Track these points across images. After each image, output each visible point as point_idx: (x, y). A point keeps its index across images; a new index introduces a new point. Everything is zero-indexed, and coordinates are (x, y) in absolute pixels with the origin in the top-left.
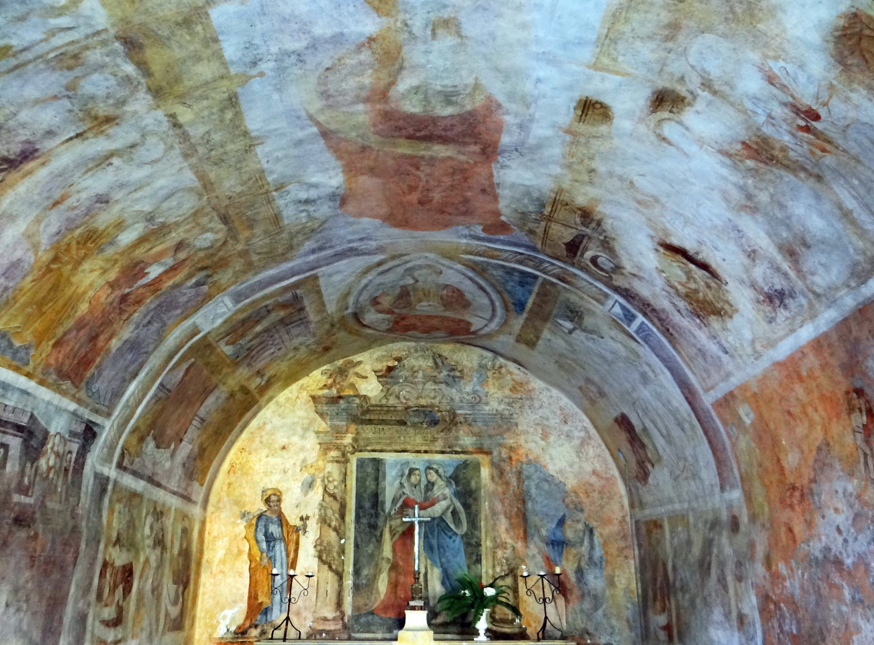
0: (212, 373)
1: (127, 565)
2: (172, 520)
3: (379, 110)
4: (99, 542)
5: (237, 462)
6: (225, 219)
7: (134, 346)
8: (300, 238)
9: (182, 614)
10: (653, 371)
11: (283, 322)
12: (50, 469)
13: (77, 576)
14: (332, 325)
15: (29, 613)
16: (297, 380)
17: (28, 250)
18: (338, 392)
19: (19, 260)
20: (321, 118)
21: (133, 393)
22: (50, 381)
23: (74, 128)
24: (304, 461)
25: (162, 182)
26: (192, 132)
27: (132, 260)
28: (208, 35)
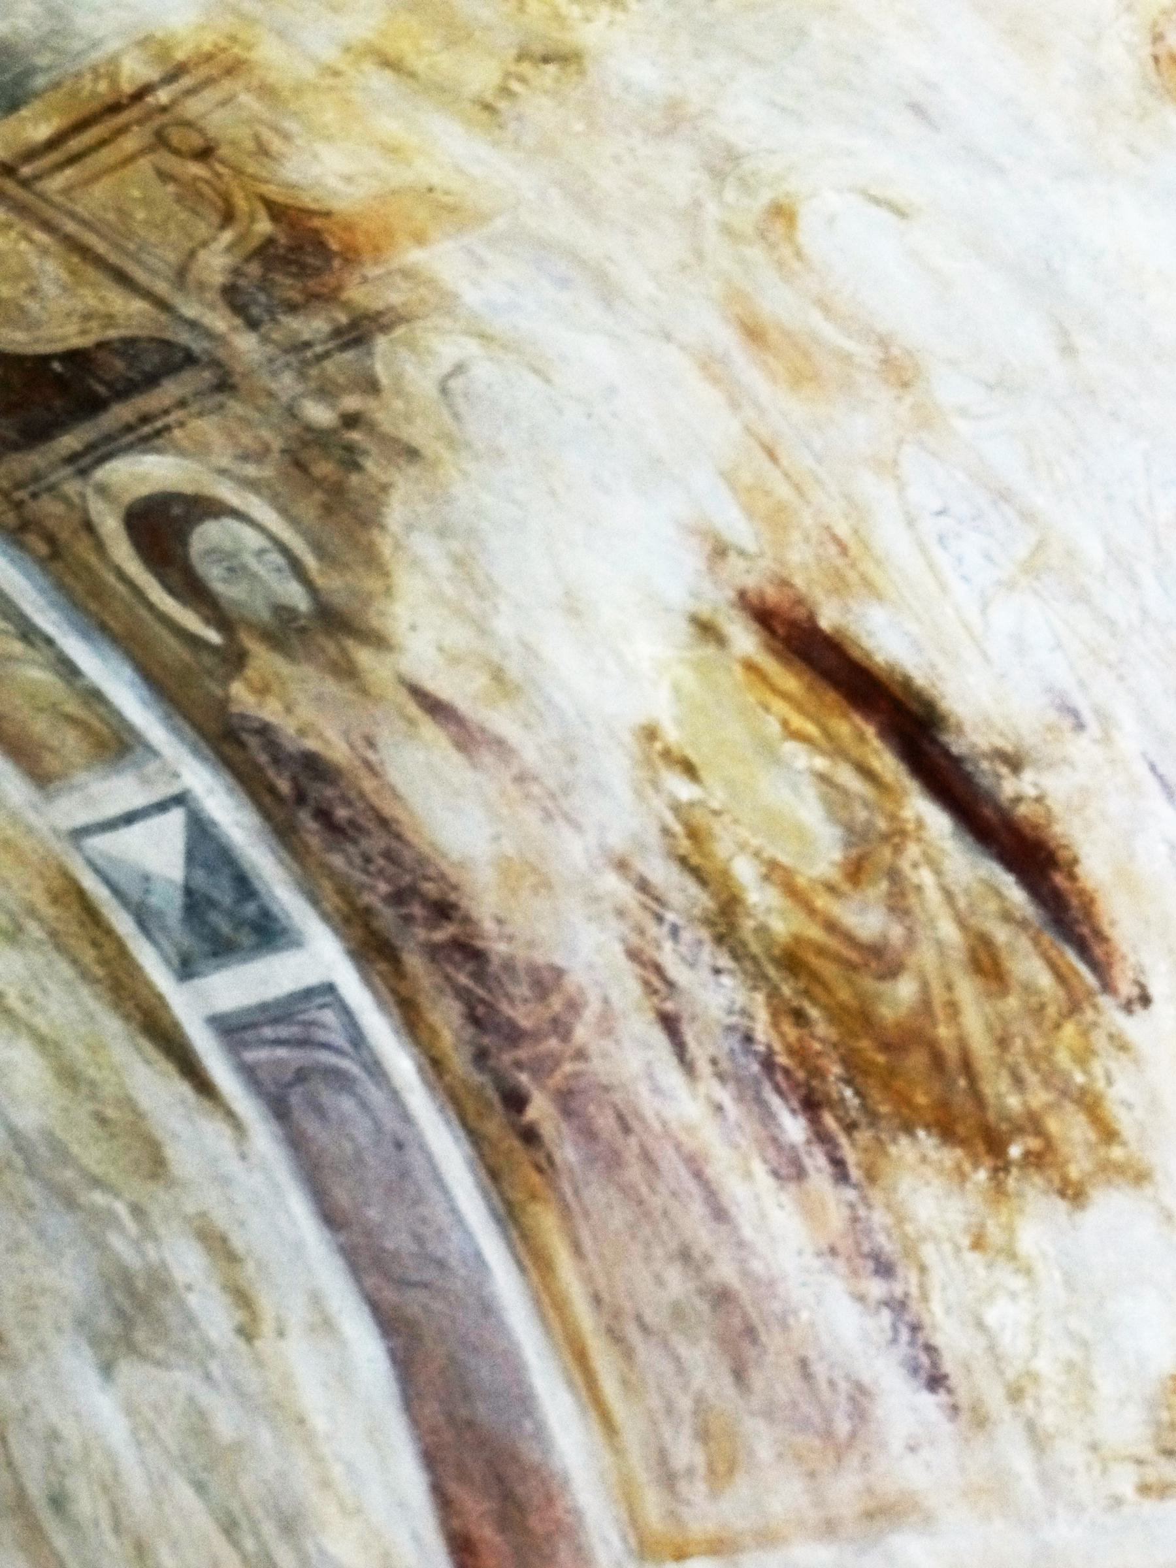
10: (242, 1298)
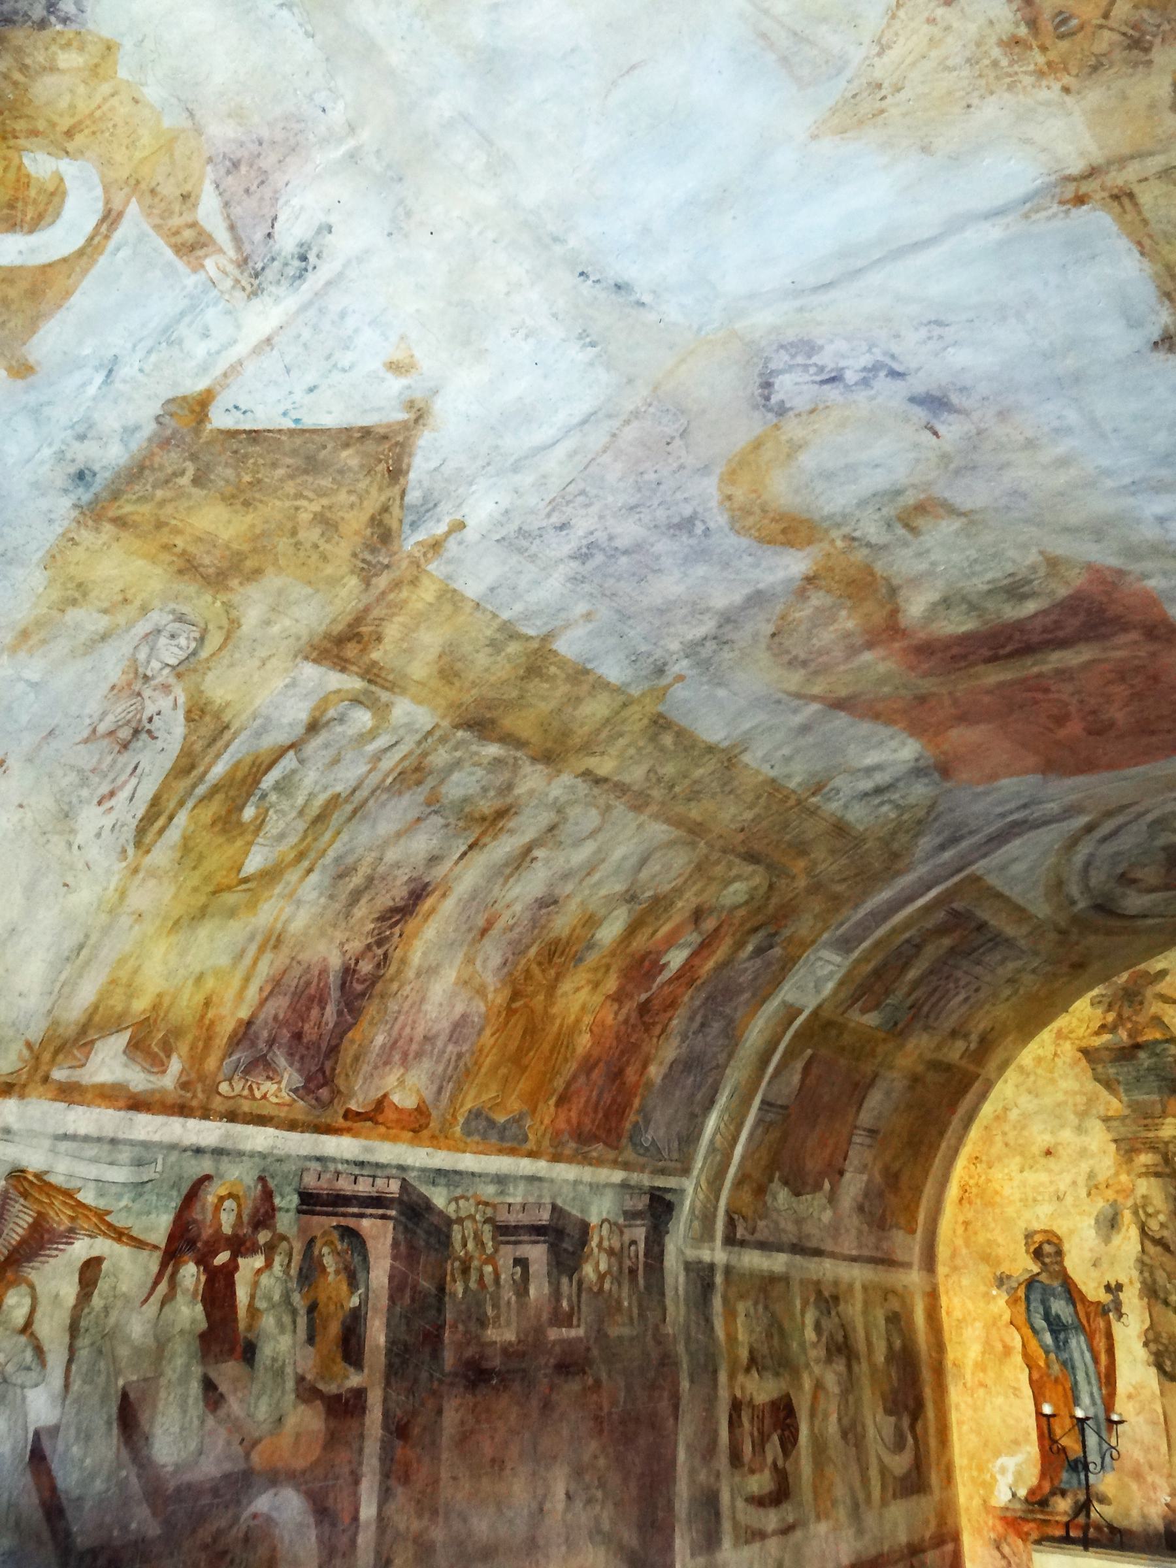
0: (858, 1059)
1: (780, 1399)
2: (859, 1306)
3: (904, 650)
4: (715, 1372)
5: (972, 1182)
6: (752, 858)
7: (689, 1064)
8: (903, 838)
9: (919, 1466)
11: (941, 970)
12: (602, 1277)
13: (686, 1433)
14: (1062, 932)
15: (610, 1506)
16: (1045, 1024)
17: (471, 999)
18: (1130, 1036)
19: (464, 1016)
20: (816, 690)
21: (717, 1130)
22: (567, 1152)
23: (461, 841)
24: (1091, 1175)
25: (618, 853)
26: (626, 778)
27: (633, 955)
28: (570, 671)
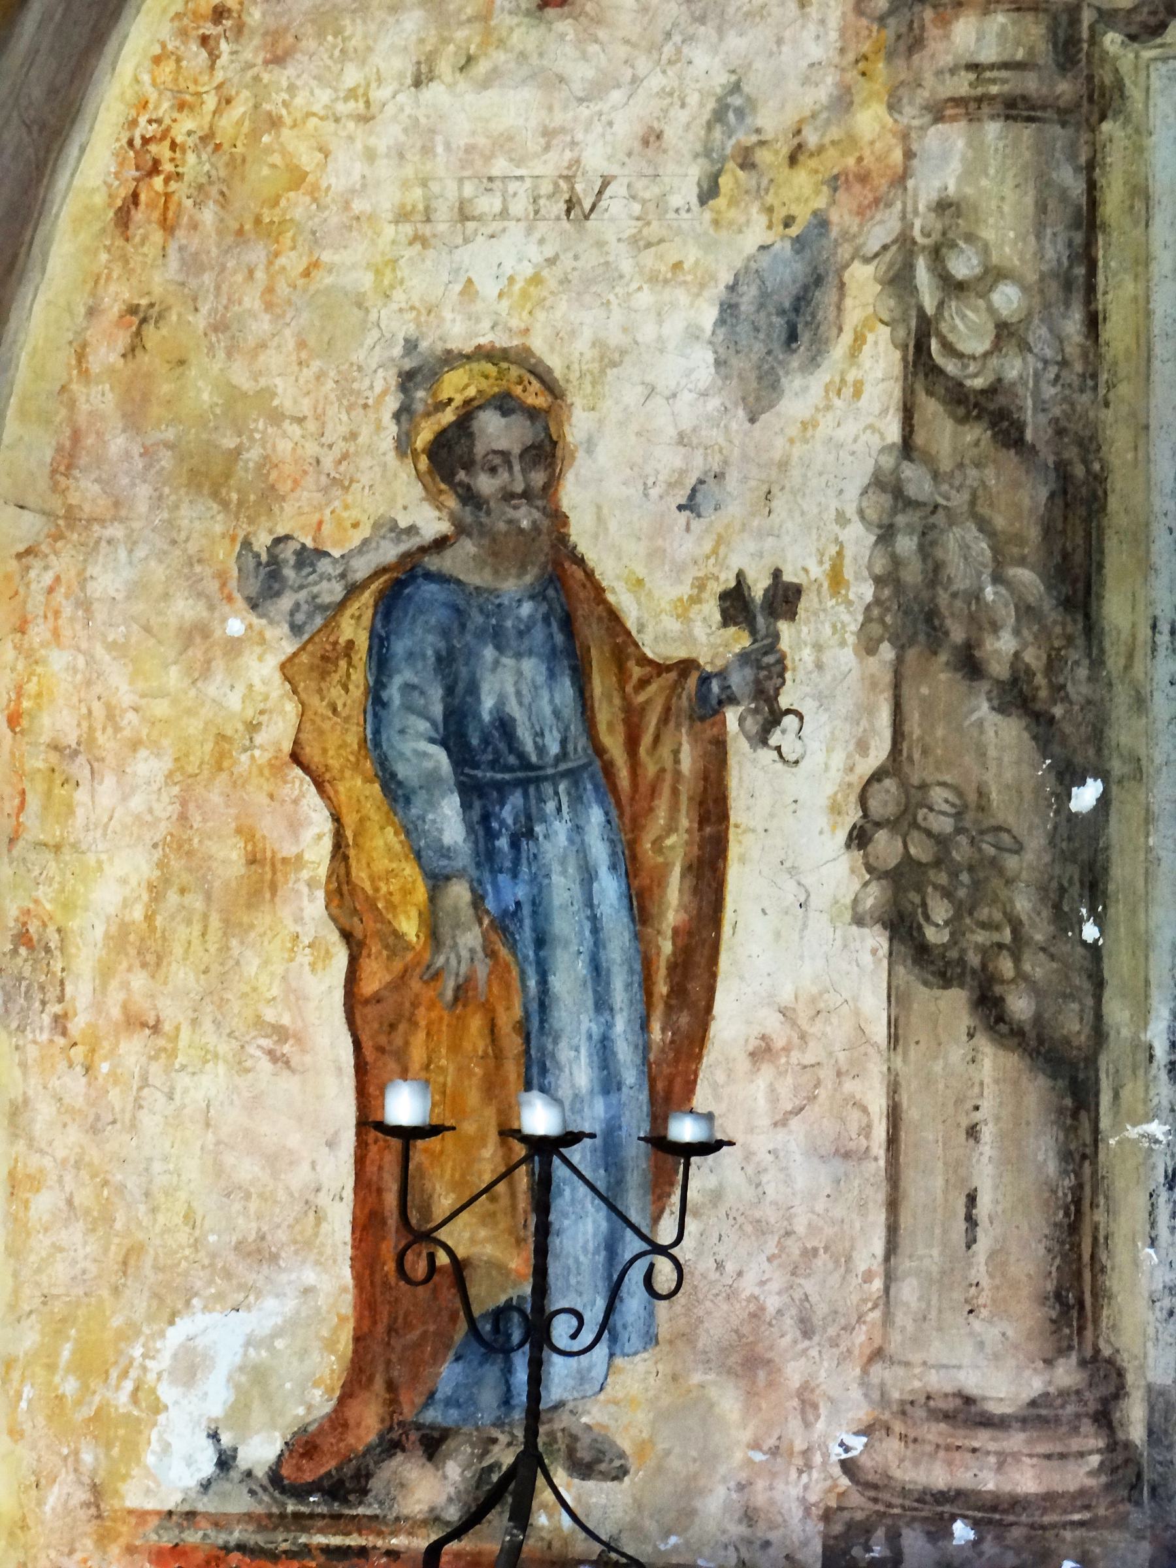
5: (185, 126)
